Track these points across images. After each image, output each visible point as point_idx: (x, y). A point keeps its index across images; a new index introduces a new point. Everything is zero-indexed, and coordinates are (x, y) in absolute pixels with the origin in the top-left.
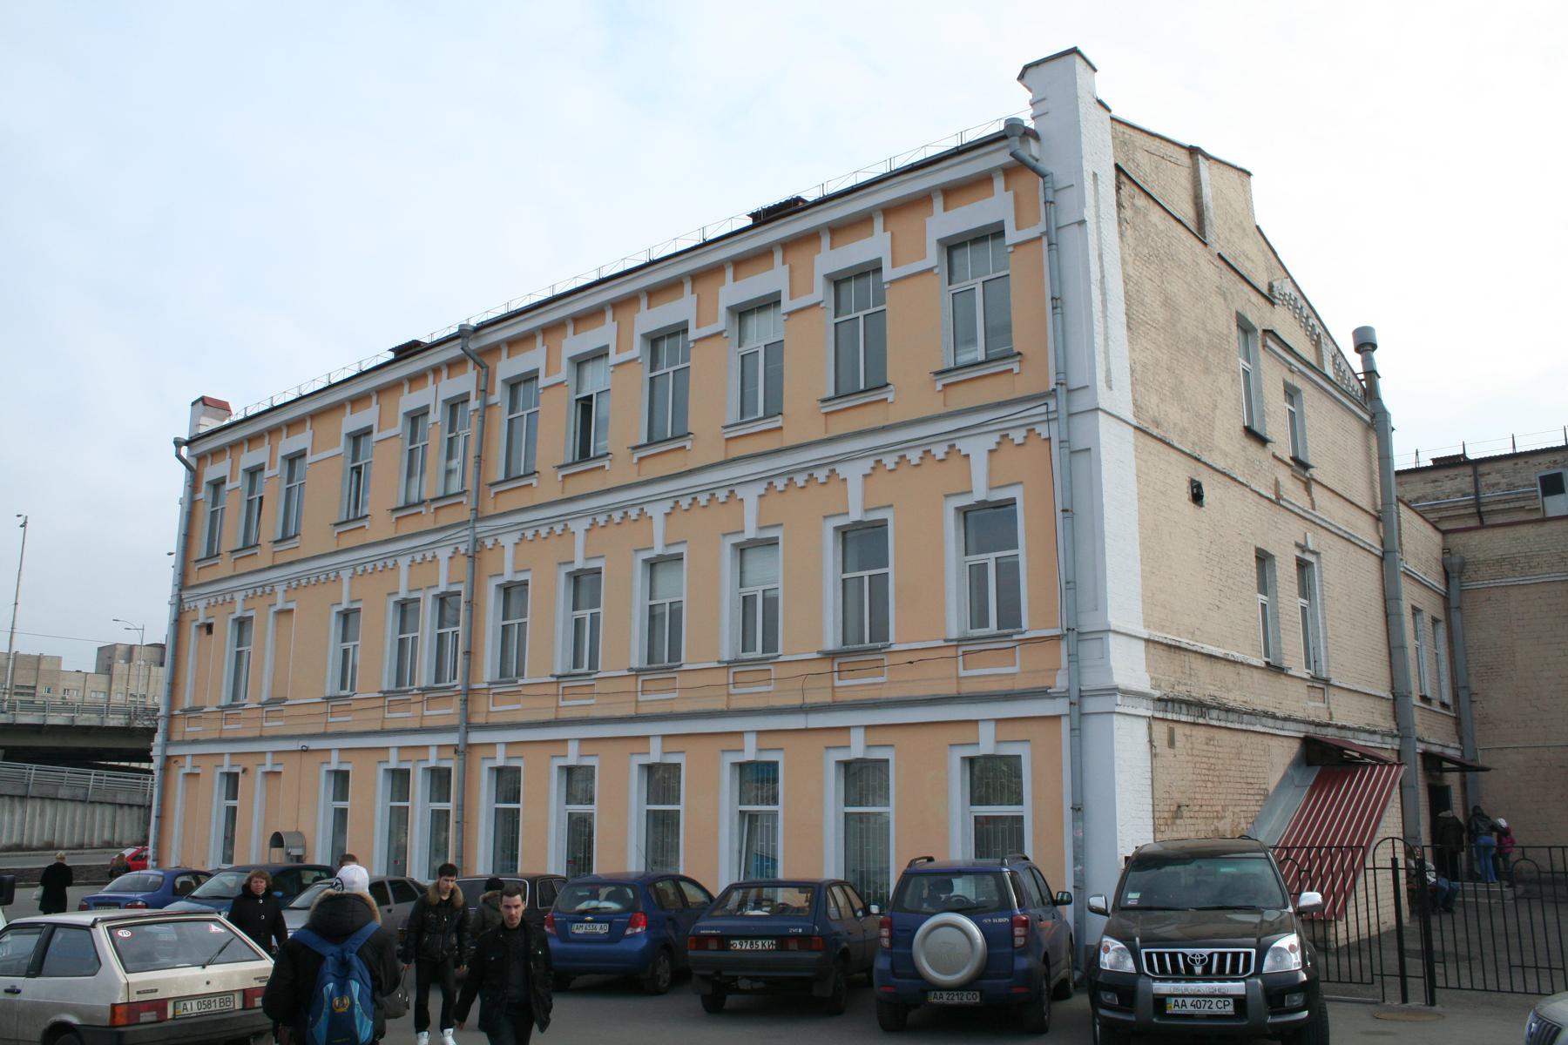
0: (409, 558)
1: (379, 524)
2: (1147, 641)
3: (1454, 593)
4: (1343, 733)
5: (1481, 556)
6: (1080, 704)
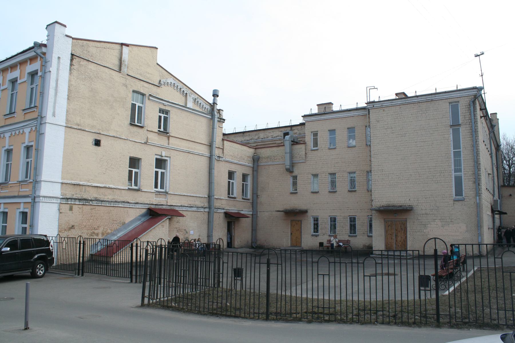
0: (10, 133)
1: (19, 116)
2: (62, 183)
3: (255, 166)
4: (172, 207)
5: (263, 156)
6: (34, 199)
